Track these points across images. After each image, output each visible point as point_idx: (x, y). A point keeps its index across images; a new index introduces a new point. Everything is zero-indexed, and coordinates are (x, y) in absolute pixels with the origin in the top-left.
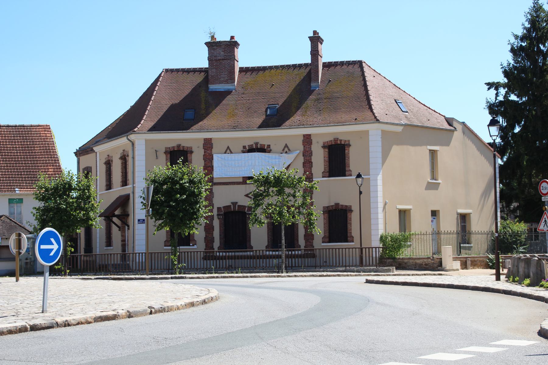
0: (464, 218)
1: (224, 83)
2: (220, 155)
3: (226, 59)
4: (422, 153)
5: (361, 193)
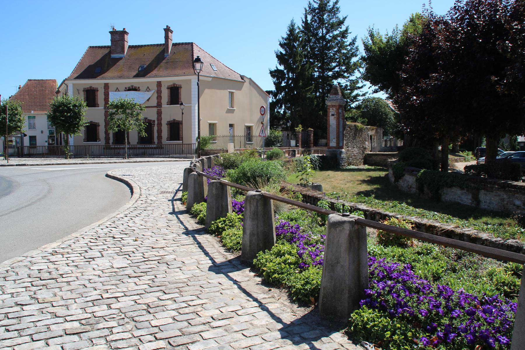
0: (249, 128)
2: (112, 92)
4: (225, 94)
5: (183, 113)
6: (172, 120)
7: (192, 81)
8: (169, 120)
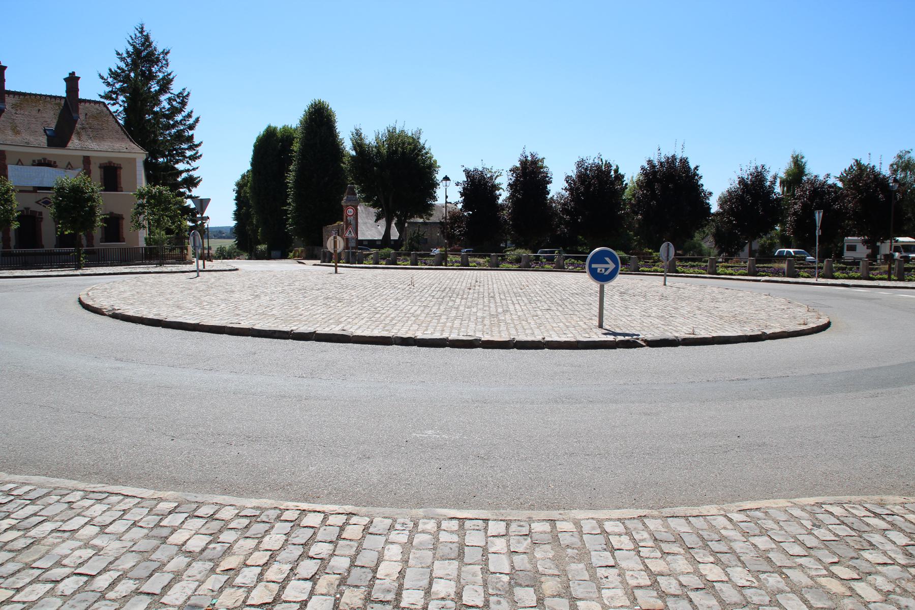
7: (137, 160)
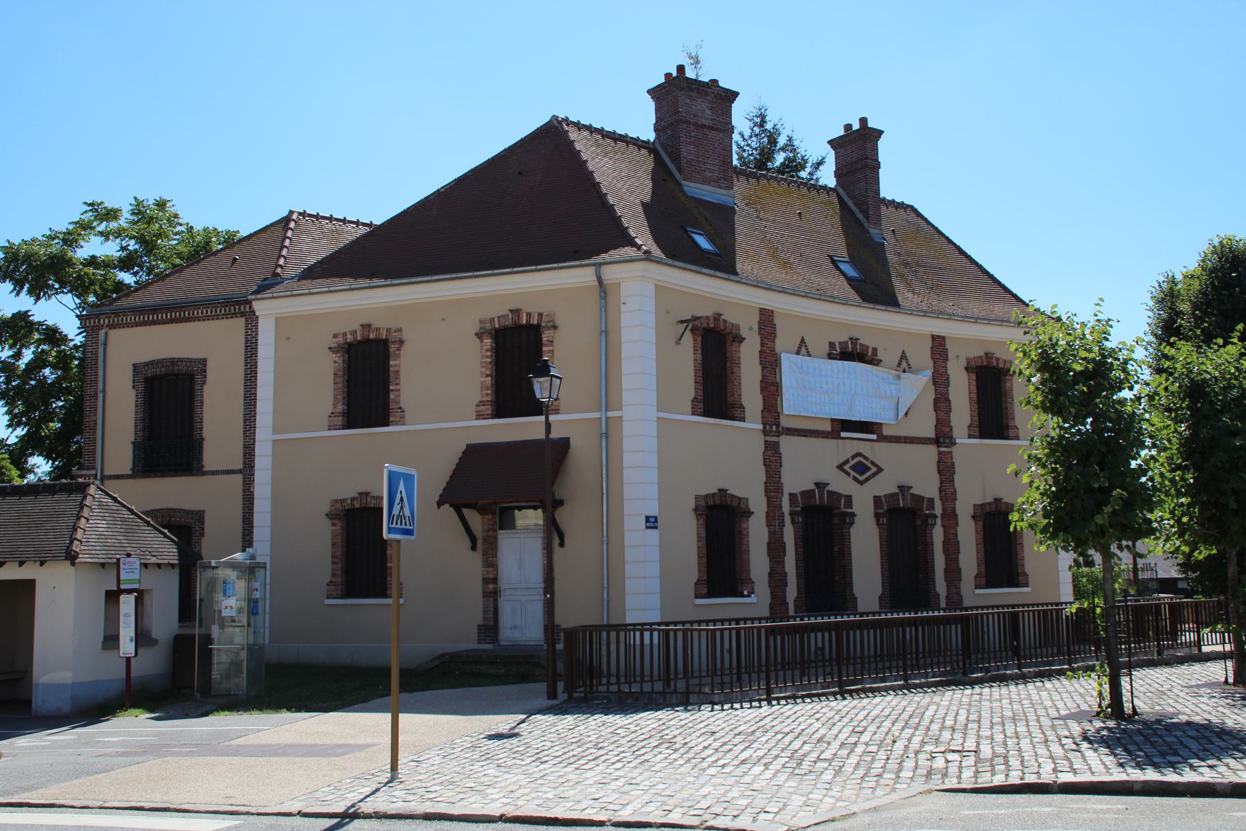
1: (713, 183)
3: (716, 129)
6: (990, 500)
8: (980, 502)
